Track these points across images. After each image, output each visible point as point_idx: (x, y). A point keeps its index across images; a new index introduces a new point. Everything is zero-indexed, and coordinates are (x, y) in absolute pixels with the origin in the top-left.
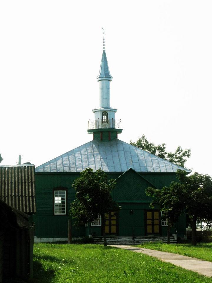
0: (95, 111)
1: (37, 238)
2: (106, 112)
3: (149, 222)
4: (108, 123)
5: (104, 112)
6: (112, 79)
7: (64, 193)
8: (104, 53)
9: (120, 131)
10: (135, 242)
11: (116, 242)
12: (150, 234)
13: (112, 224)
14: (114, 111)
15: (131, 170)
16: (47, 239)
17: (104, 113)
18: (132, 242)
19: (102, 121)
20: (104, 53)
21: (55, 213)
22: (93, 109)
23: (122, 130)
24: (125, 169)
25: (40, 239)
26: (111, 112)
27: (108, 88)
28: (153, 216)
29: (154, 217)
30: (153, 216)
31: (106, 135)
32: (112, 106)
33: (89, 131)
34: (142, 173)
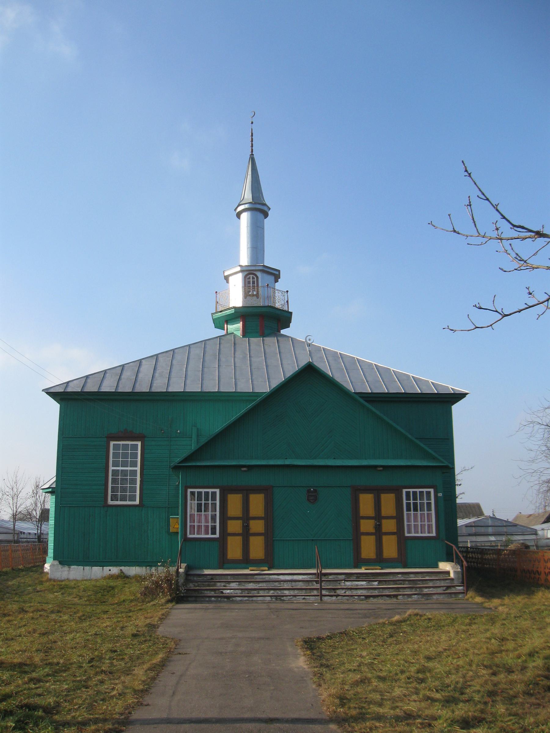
1: (60, 566)
4: (258, 298)
7: (135, 447)
8: (252, 159)
12: (257, 563)
16: (87, 568)
17: (248, 277)
18: (315, 593)
25: (66, 568)
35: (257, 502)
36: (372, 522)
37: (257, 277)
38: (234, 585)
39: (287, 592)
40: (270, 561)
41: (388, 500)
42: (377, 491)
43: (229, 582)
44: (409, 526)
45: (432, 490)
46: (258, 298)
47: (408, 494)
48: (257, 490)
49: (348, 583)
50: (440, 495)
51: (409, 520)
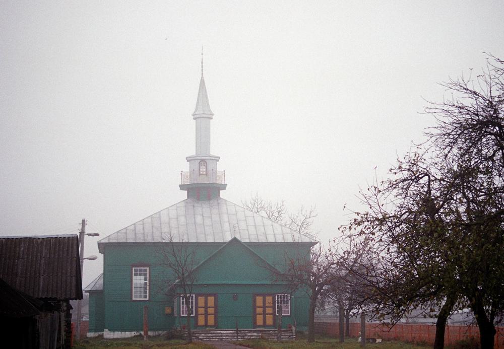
0: (189, 159)
1: (109, 332)
2: (202, 161)
3: (259, 310)
4: (207, 175)
5: (202, 160)
6: (214, 117)
7: (145, 270)
8: (202, 82)
9: (224, 187)
10: (239, 337)
11: (214, 337)
12: (211, 326)
13: (208, 313)
14: (217, 159)
15: (235, 240)
16: (123, 333)
19: (200, 173)
20: (202, 82)
21: (133, 297)
22: (188, 155)
23: (226, 185)
24: (228, 238)
25: (112, 333)
26: (211, 161)
27: (208, 129)
28: (206, 303)
29: (207, 304)
30: (206, 303)
31: (203, 191)
32: (213, 152)
33: (182, 187)
34: (251, 244)
35: (211, 300)
36: (203, 309)
37: (206, 163)
38: (203, 335)
39: (224, 337)
40: (216, 326)
41: (269, 299)
42: (264, 296)
43: (201, 334)
44: (285, 311)
45: (182, 315)
46: (207, 175)
47: (278, 296)
48: (210, 295)
49: (249, 334)
50: (293, 297)
51: (183, 309)
